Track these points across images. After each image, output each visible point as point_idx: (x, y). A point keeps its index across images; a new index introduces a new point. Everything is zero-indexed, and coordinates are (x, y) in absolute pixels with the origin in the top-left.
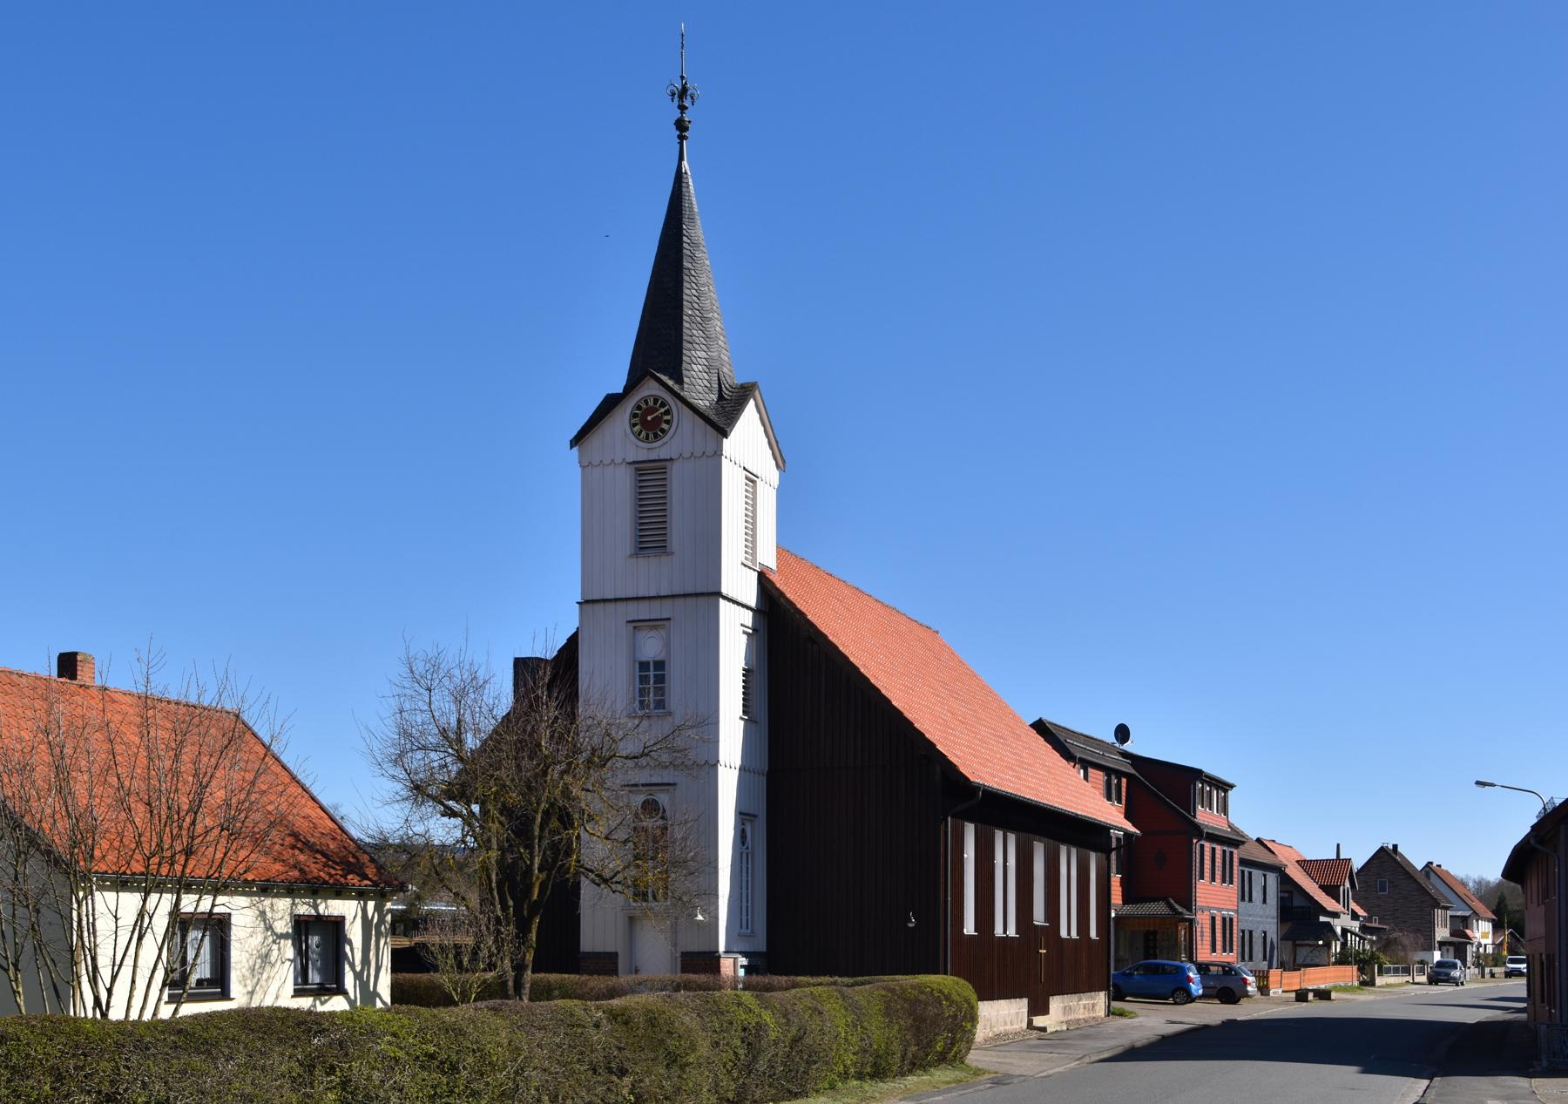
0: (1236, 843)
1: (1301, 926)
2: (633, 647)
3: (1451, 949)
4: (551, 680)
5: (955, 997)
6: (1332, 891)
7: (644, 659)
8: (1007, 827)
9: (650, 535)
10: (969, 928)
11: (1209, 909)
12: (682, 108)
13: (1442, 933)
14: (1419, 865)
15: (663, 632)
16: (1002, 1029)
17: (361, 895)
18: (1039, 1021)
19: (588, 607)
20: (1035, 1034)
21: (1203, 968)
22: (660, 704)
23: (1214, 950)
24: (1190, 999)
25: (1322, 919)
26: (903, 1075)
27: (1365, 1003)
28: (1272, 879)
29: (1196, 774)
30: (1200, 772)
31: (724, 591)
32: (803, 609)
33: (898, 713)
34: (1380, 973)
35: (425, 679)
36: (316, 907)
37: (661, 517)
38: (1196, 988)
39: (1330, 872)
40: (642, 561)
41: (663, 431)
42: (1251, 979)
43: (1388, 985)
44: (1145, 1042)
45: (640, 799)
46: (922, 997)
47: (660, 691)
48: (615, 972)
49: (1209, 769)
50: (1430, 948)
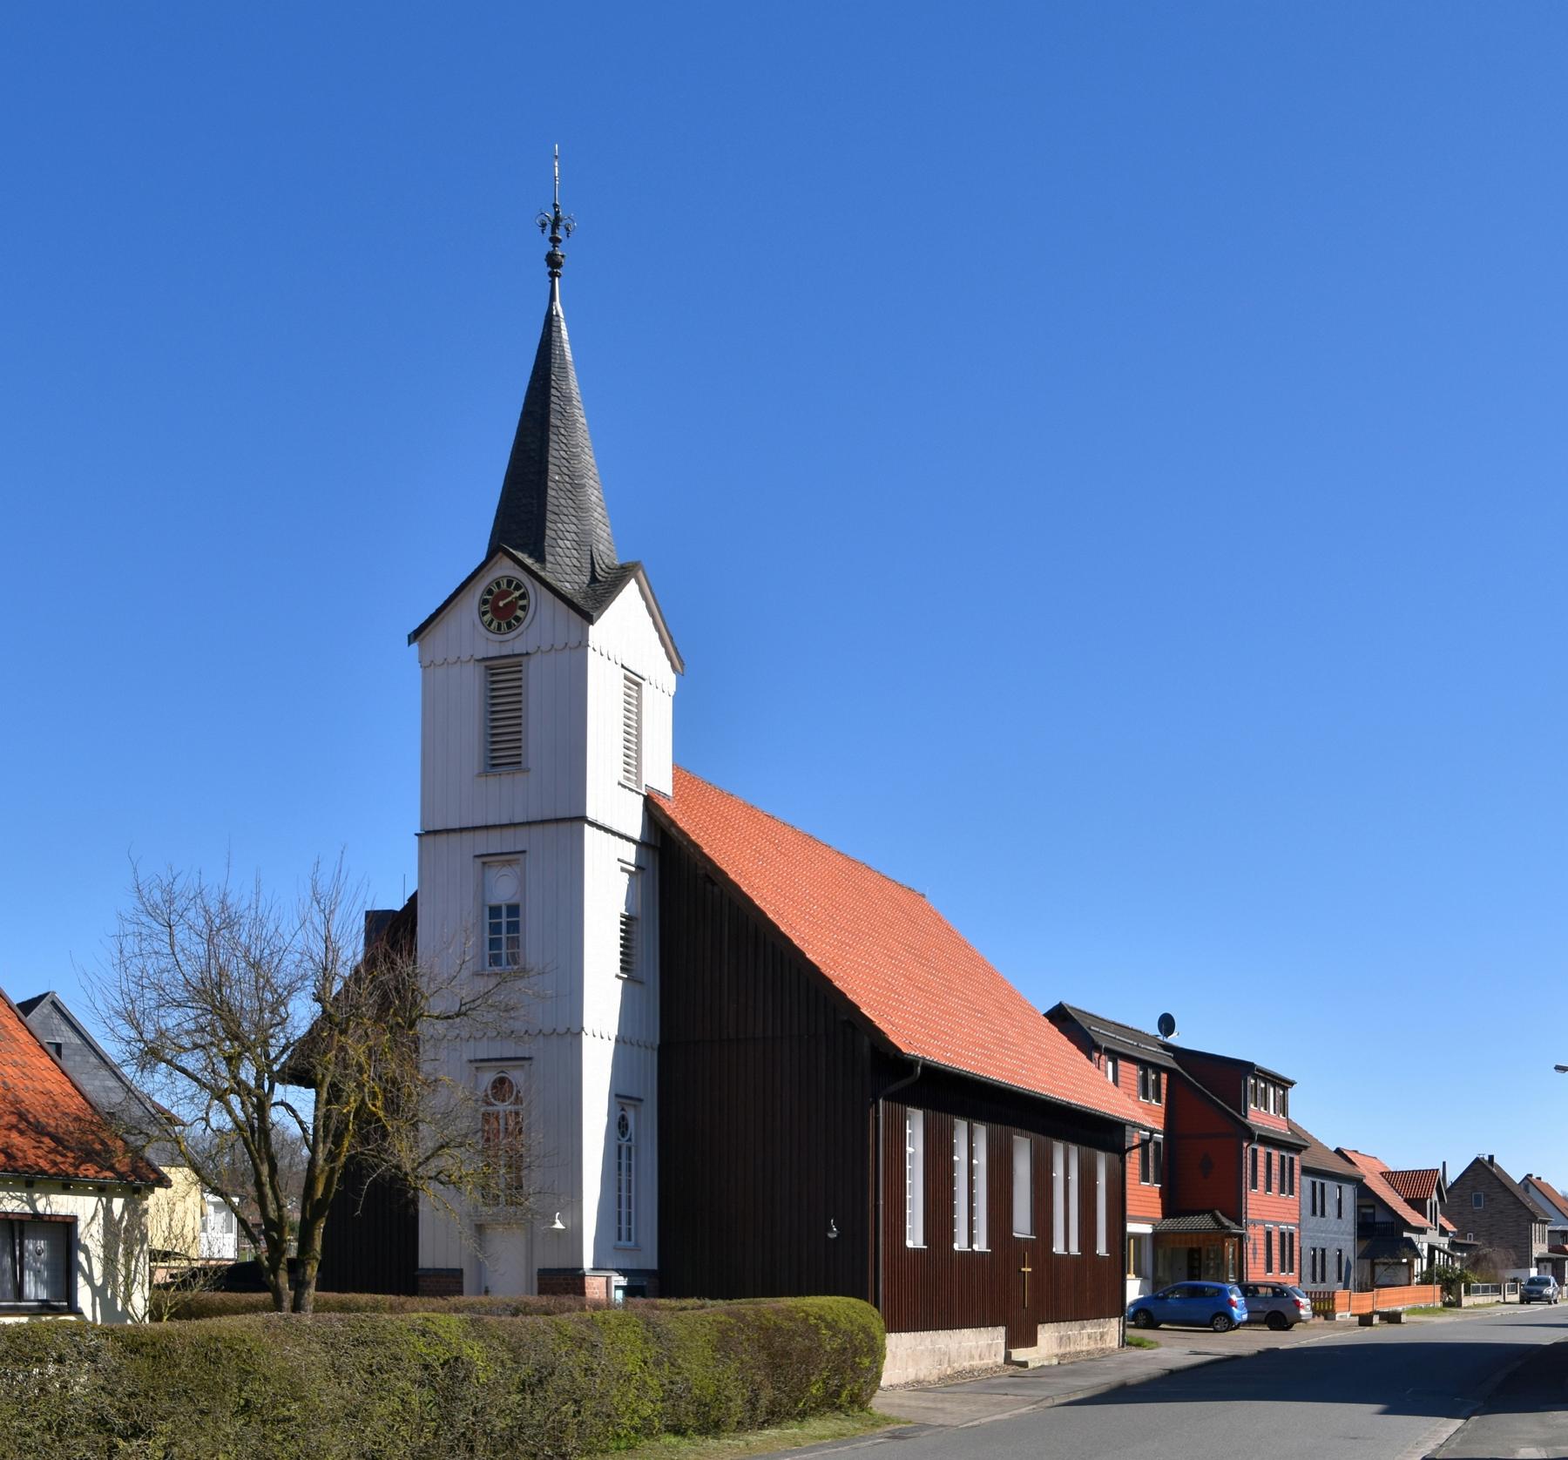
0: (1298, 1149)
1: (1381, 1239)
2: (482, 887)
3: (1549, 1266)
4: (393, 931)
5: (844, 1325)
6: (1417, 1204)
7: (494, 902)
8: (973, 1115)
9: (503, 749)
10: (915, 1239)
11: (1263, 1222)
12: (555, 241)
13: (1540, 1249)
14: (1518, 1178)
15: (517, 869)
16: (966, 1364)
17: (101, 1190)
18: (1019, 1354)
19: (431, 839)
20: (1011, 1369)
21: (1249, 1291)
22: (514, 959)
23: (1269, 1269)
24: (1231, 1325)
25: (1406, 1235)
26: (761, 1427)
27: (1443, 1325)
28: (1349, 1191)
29: (1247, 1068)
30: (1251, 1065)
31: (591, 814)
32: (698, 841)
33: (813, 969)
34: (1467, 1292)
35: (163, 913)
36: (32, 1203)
37: (516, 727)
38: (1240, 1314)
39: (1416, 1185)
40: (492, 780)
41: (518, 619)
42: (1304, 1301)
43: (1476, 1306)
44: (1144, 1378)
45: (488, 1077)
46: (786, 1324)
47: (514, 942)
48: (460, 1292)
49: (1261, 1062)
50: (1528, 1265)
